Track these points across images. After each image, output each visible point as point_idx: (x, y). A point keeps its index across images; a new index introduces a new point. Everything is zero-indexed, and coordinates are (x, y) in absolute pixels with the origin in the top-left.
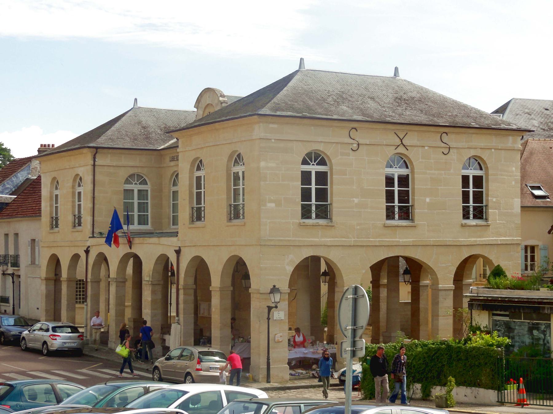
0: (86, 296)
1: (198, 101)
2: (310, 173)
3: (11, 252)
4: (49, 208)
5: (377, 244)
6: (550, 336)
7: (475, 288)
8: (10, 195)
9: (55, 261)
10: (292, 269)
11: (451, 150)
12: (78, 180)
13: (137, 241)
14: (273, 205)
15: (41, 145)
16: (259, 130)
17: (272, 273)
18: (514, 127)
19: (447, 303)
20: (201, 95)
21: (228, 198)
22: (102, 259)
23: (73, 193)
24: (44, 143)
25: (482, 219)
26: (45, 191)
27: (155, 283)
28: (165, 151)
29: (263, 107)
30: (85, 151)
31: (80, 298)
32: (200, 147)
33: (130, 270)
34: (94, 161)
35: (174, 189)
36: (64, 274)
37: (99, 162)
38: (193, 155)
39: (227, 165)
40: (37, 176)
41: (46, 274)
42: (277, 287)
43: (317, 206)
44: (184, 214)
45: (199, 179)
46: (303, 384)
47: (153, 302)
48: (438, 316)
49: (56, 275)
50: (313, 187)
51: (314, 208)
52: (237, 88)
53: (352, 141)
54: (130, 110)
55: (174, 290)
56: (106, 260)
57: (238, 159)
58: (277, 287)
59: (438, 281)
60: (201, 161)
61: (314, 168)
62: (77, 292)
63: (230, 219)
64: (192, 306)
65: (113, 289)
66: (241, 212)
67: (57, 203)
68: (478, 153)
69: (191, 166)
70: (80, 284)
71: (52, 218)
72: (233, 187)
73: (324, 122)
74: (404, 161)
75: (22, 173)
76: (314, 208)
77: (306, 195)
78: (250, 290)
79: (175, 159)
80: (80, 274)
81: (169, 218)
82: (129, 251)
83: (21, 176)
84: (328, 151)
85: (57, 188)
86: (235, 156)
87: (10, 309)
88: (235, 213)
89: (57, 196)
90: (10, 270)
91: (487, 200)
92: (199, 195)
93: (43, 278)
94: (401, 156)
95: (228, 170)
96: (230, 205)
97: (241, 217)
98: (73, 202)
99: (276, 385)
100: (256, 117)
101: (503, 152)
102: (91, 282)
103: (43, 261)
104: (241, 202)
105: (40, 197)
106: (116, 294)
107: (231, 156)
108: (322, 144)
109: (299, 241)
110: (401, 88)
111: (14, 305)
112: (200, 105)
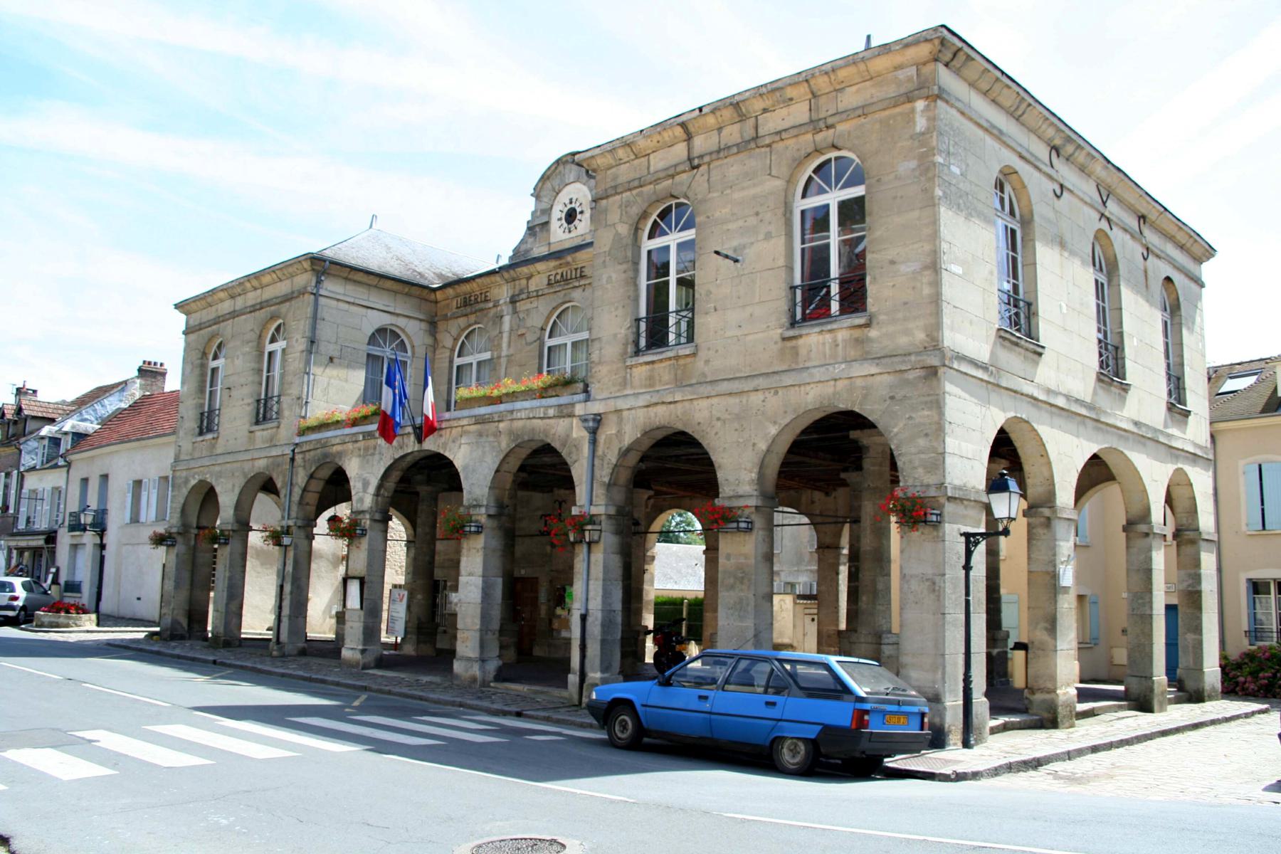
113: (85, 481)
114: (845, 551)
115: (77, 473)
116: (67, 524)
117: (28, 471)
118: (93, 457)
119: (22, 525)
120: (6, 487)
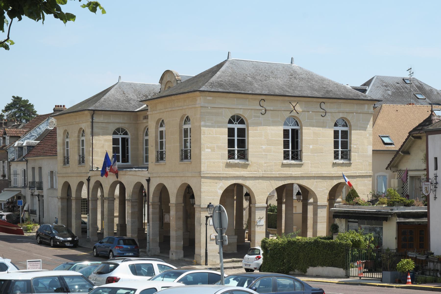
0: (89, 210)
1: (162, 78)
2: (234, 129)
3: (37, 180)
4: (62, 151)
5: (278, 176)
6: (382, 235)
7: (340, 204)
8: (35, 140)
9: (67, 187)
10: (222, 192)
11: (327, 114)
12: (82, 132)
13: (120, 173)
14: (210, 150)
15: (56, 106)
16: (200, 101)
17: (210, 194)
18: (369, 98)
19: (323, 214)
20: (164, 74)
21: (181, 146)
22: (99, 185)
23: (79, 141)
24: (57, 105)
25: (347, 159)
26: (59, 139)
27: (133, 201)
28: (140, 112)
29: (203, 84)
30: (86, 112)
31: (84, 211)
32: (162, 111)
33: (117, 192)
34: (92, 119)
35: (146, 138)
36: (74, 195)
37: (95, 119)
38: (157, 117)
39: (180, 124)
40: (54, 127)
41: (61, 195)
42: (212, 204)
43: (238, 151)
44: (152, 155)
45: (161, 132)
46: (228, 266)
47: (133, 213)
48: (317, 222)
49: (68, 195)
50: (236, 138)
51: (236, 152)
52: (187, 70)
53: (261, 108)
54: (116, 84)
55: (146, 206)
56: (101, 185)
57: (187, 119)
58: (212, 204)
59: (317, 200)
60: (163, 121)
61: (236, 126)
62: (82, 206)
63: (182, 159)
64: (158, 216)
65: (106, 205)
66: (189, 155)
67: (67, 147)
68: (344, 115)
69: (156, 124)
70: (84, 202)
71: (65, 157)
72: (183, 139)
73: (243, 96)
74: (296, 121)
75: (43, 125)
76: (236, 152)
77: (231, 143)
78: (195, 206)
79: (146, 117)
80: (84, 194)
81: (143, 158)
82: (116, 180)
83: (43, 127)
84: (245, 115)
85: (67, 137)
86: (185, 118)
87: (37, 219)
88: (185, 155)
89: (67, 142)
90: (36, 192)
91: (350, 147)
92: (162, 143)
93: (59, 198)
94: (294, 118)
95: (181, 127)
96: (182, 150)
97: (189, 158)
98: (79, 146)
99: (211, 267)
100: (198, 92)
101: (361, 115)
102: (92, 200)
103: (59, 185)
104: (189, 148)
105: (56, 142)
106: (108, 208)
107: (182, 118)
108: (242, 110)
109: (226, 174)
110: (295, 72)
111: (39, 216)
112: (163, 82)
113: (33, 168)
114: (300, 238)
115: (30, 165)
116: (28, 186)
117: (11, 161)
118: (35, 159)
119: (12, 184)
120: (4, 167)
